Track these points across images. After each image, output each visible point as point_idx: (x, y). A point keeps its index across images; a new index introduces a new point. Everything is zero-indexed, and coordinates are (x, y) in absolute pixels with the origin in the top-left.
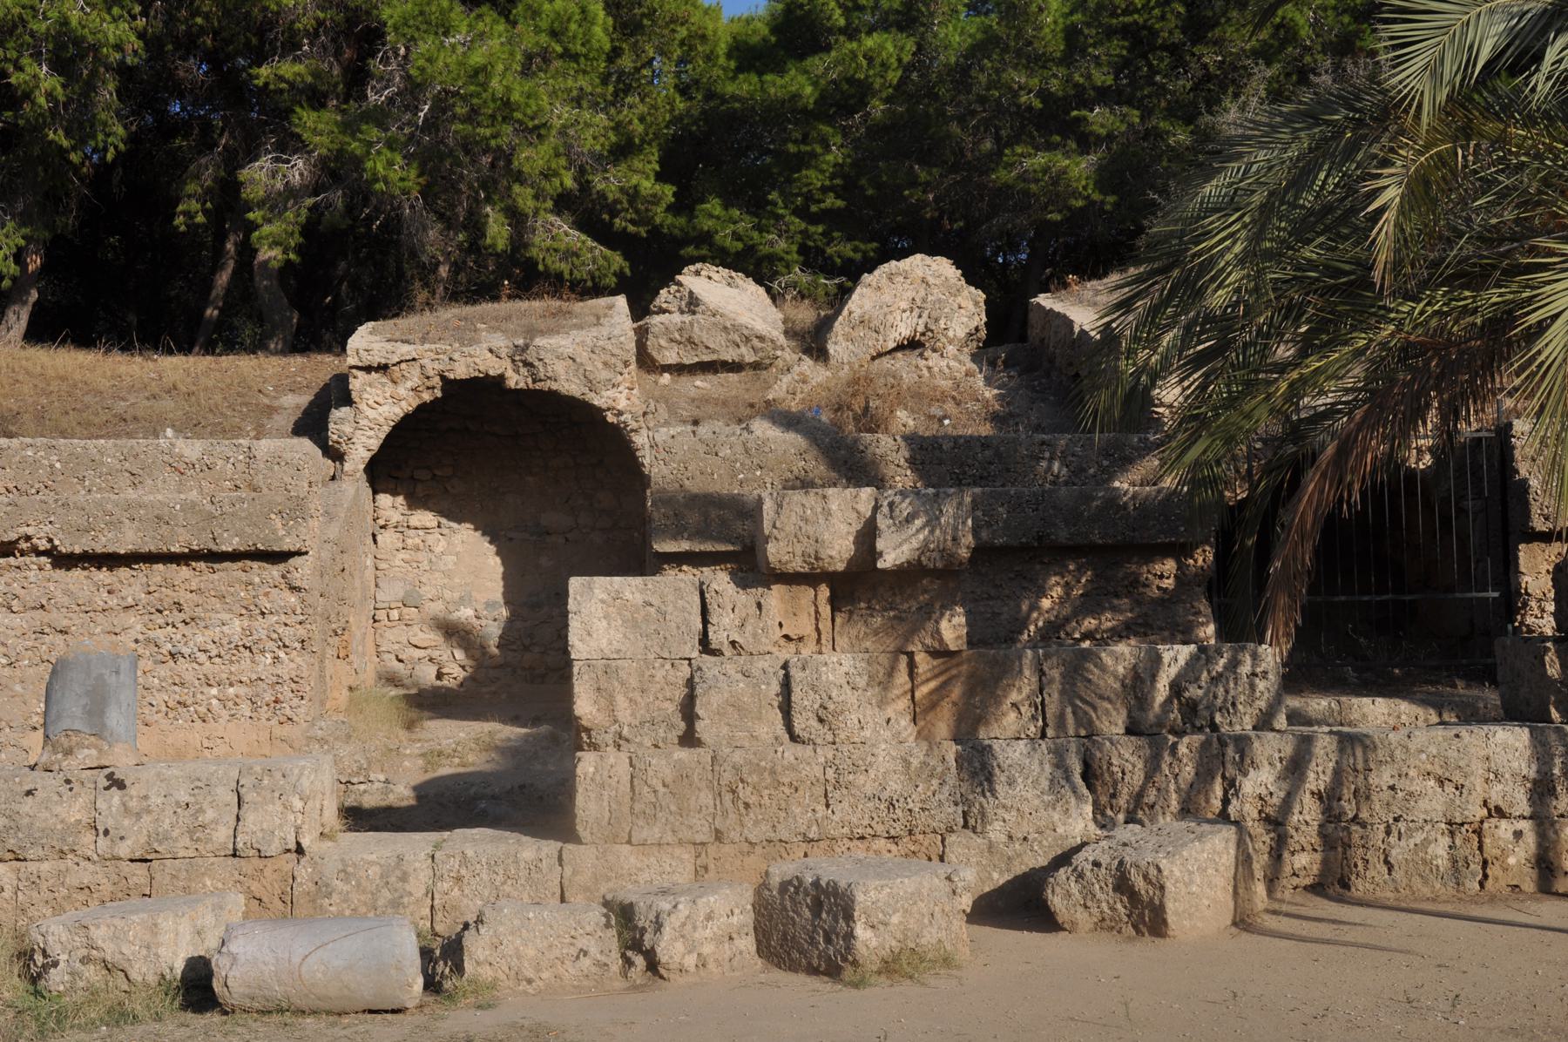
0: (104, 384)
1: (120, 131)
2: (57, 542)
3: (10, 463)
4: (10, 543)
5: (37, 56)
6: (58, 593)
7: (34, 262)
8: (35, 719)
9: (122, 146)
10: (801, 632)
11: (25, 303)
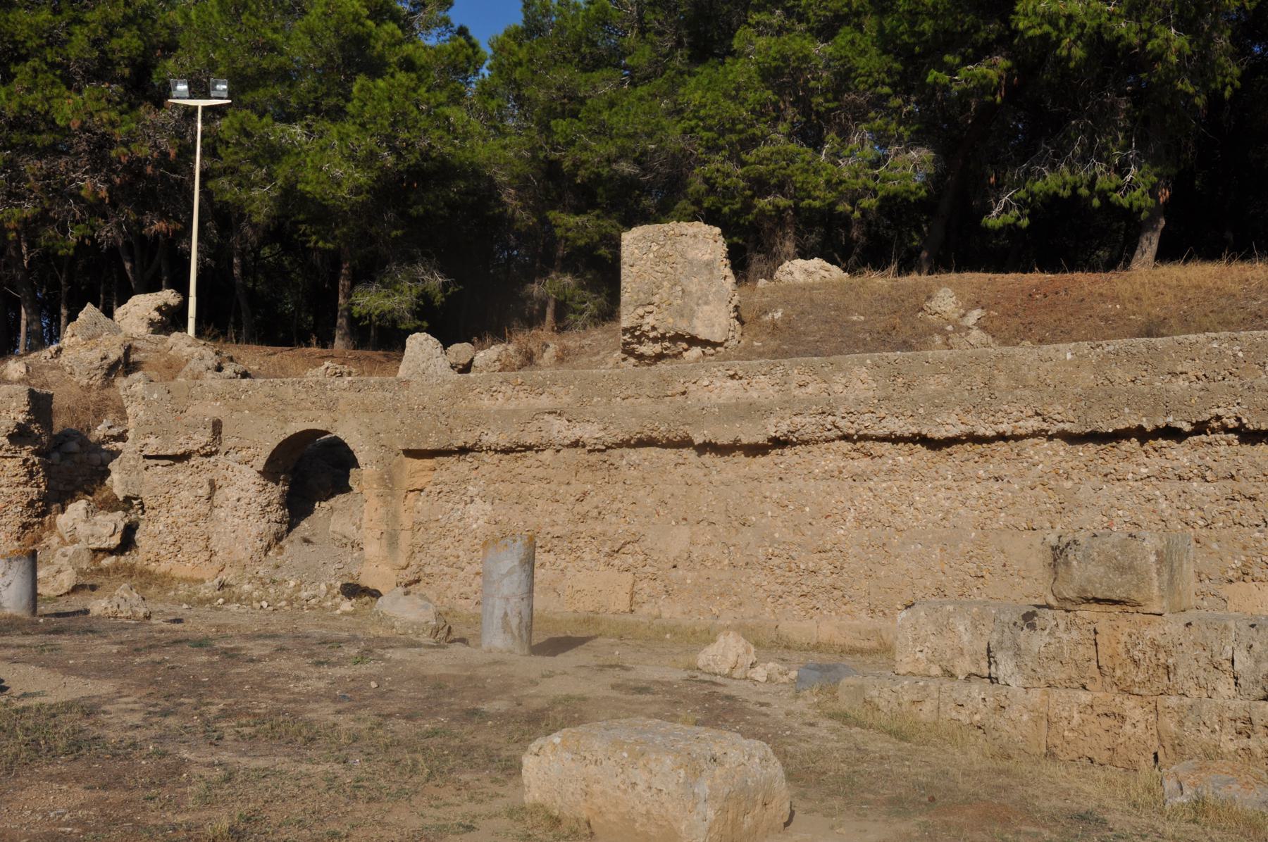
0: (1235, 288)
1: (1236, 71)
2: (1245, 421)
3: (1199, 355)
4: (1204, 422)
5: (1165, 22)
6: (1246, 465)
7: (1164, 195)
8: (1231, 573)
9: (1237, 84)
10: (149, 472)
11: (1155, 230)
